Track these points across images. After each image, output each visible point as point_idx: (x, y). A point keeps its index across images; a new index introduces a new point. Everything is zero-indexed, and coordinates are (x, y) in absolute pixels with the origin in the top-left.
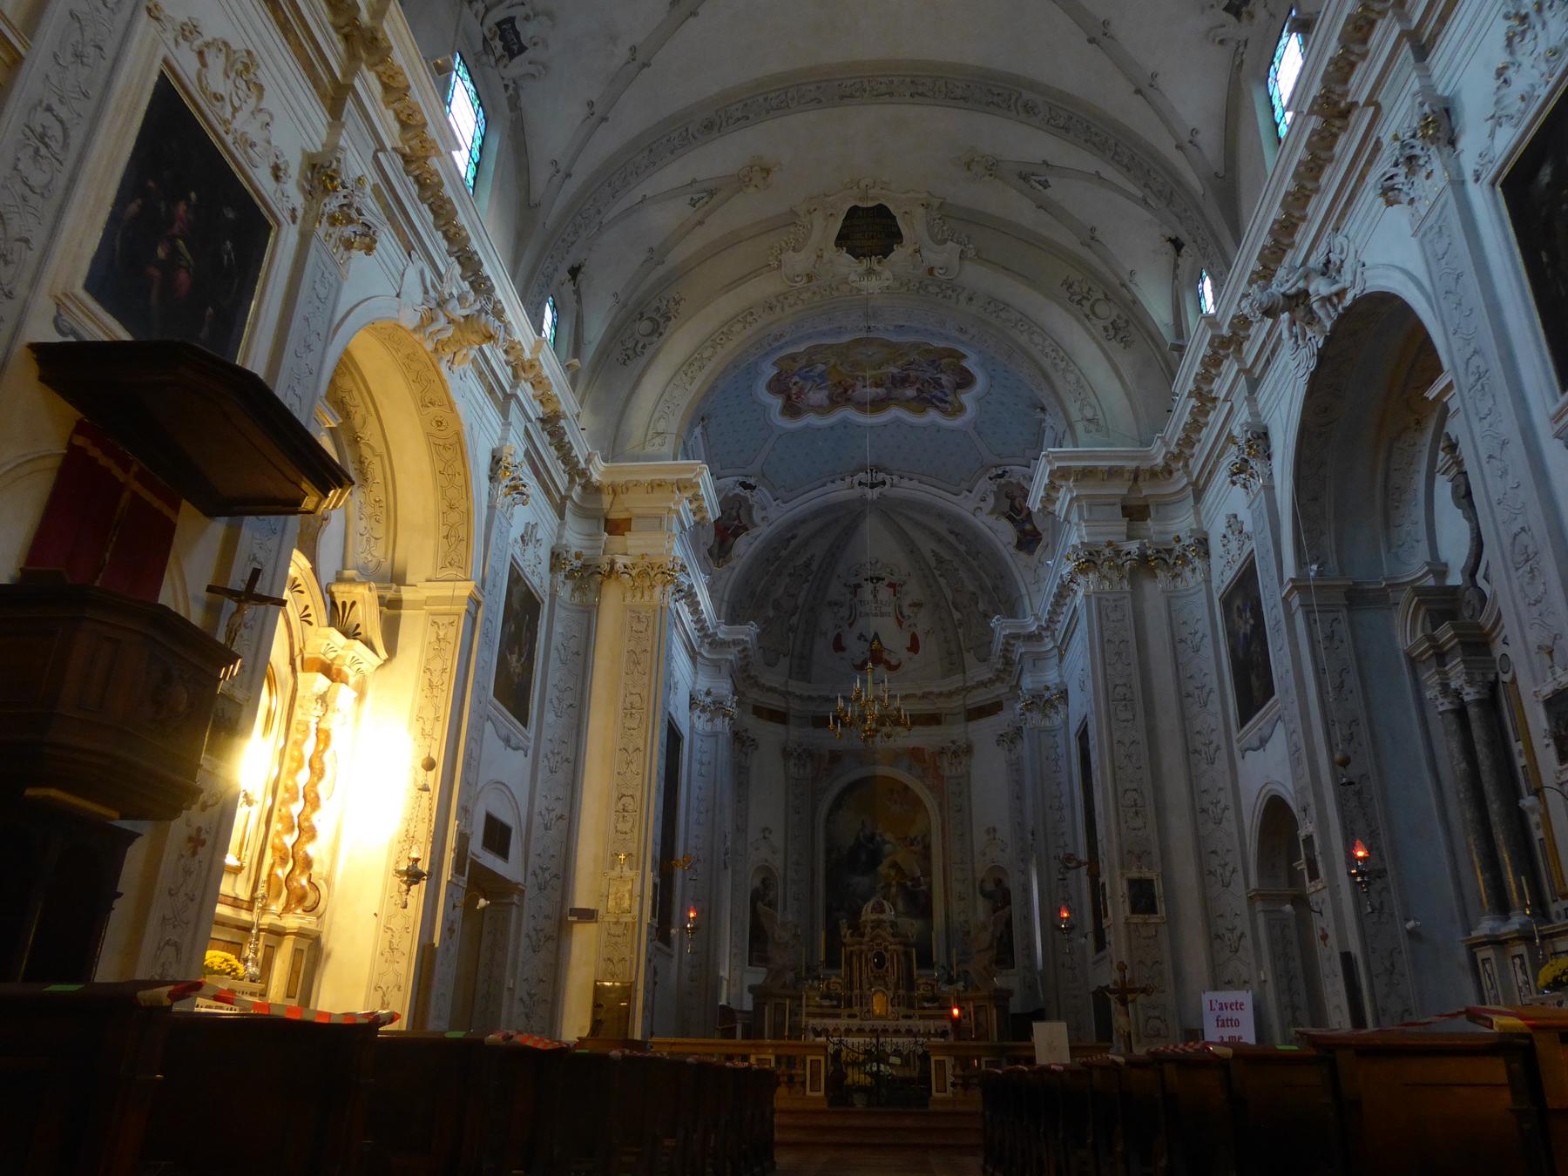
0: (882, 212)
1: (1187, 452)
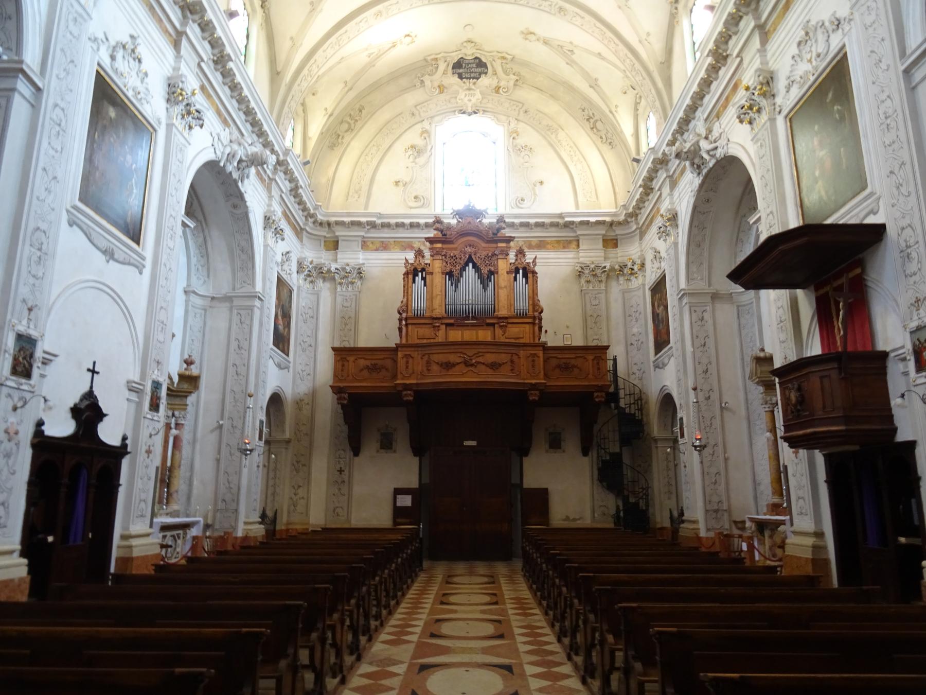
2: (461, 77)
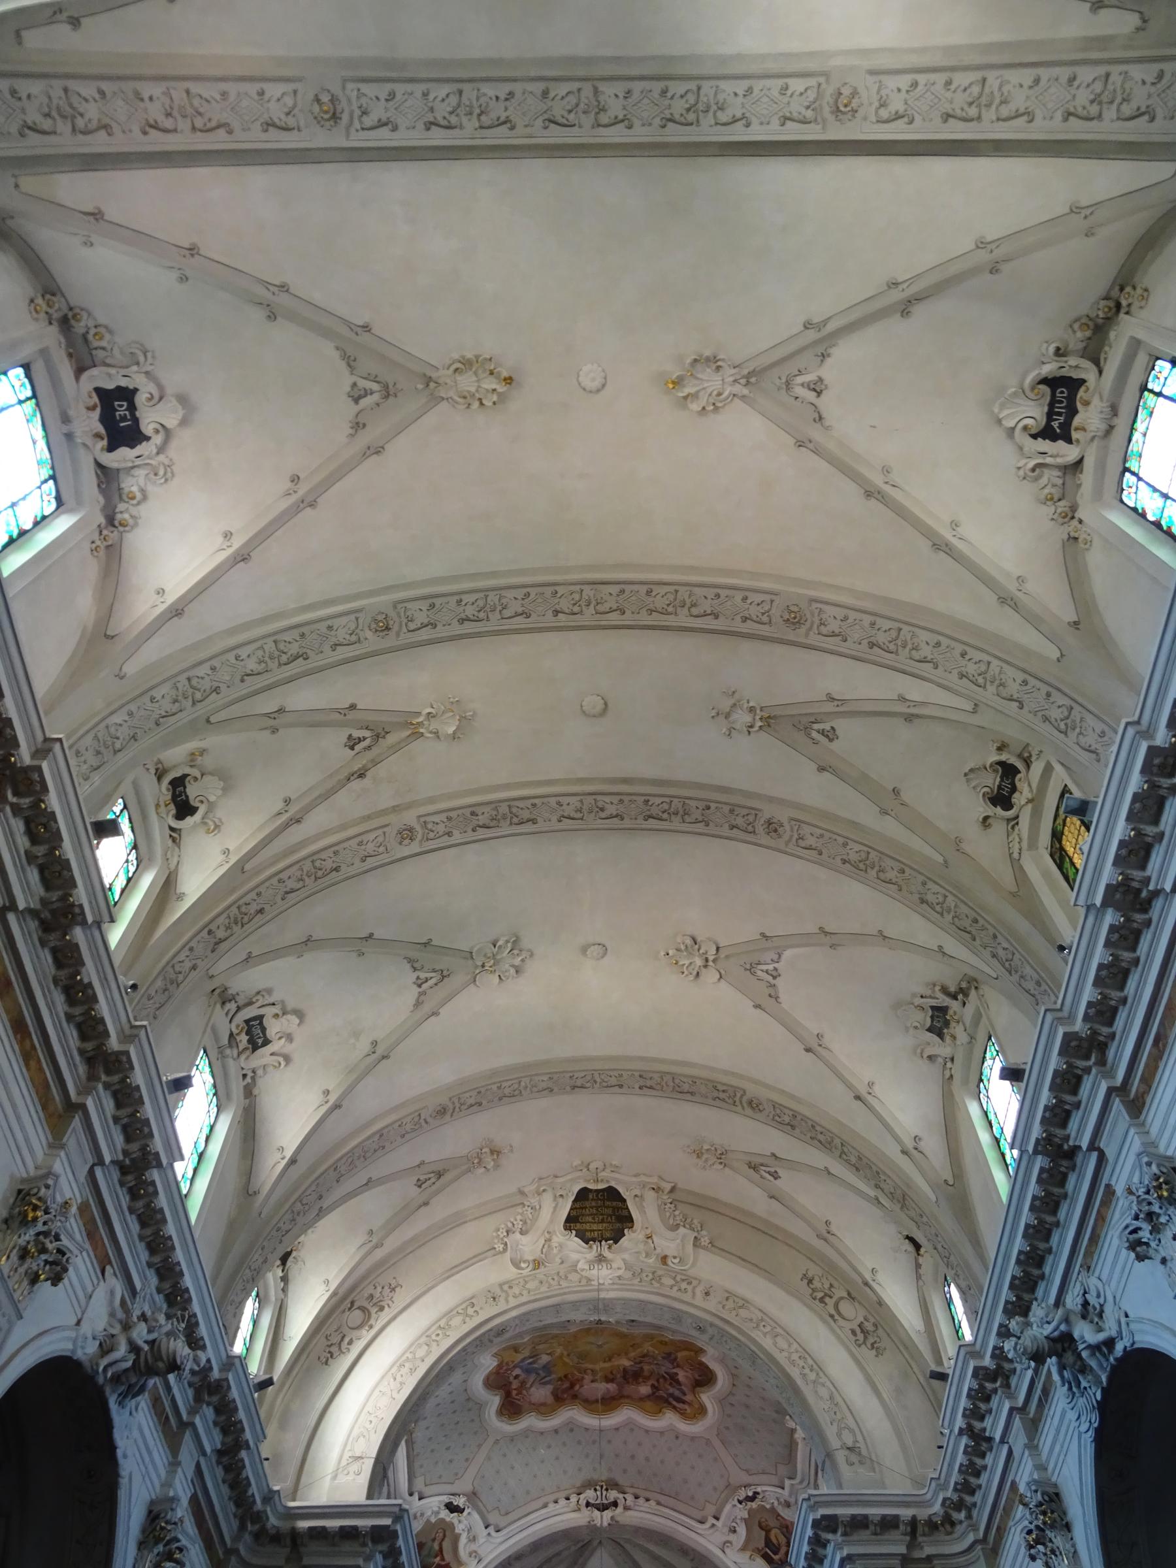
0: (612, 1194)
1: (968, 1499)
2: (581, 1235)
